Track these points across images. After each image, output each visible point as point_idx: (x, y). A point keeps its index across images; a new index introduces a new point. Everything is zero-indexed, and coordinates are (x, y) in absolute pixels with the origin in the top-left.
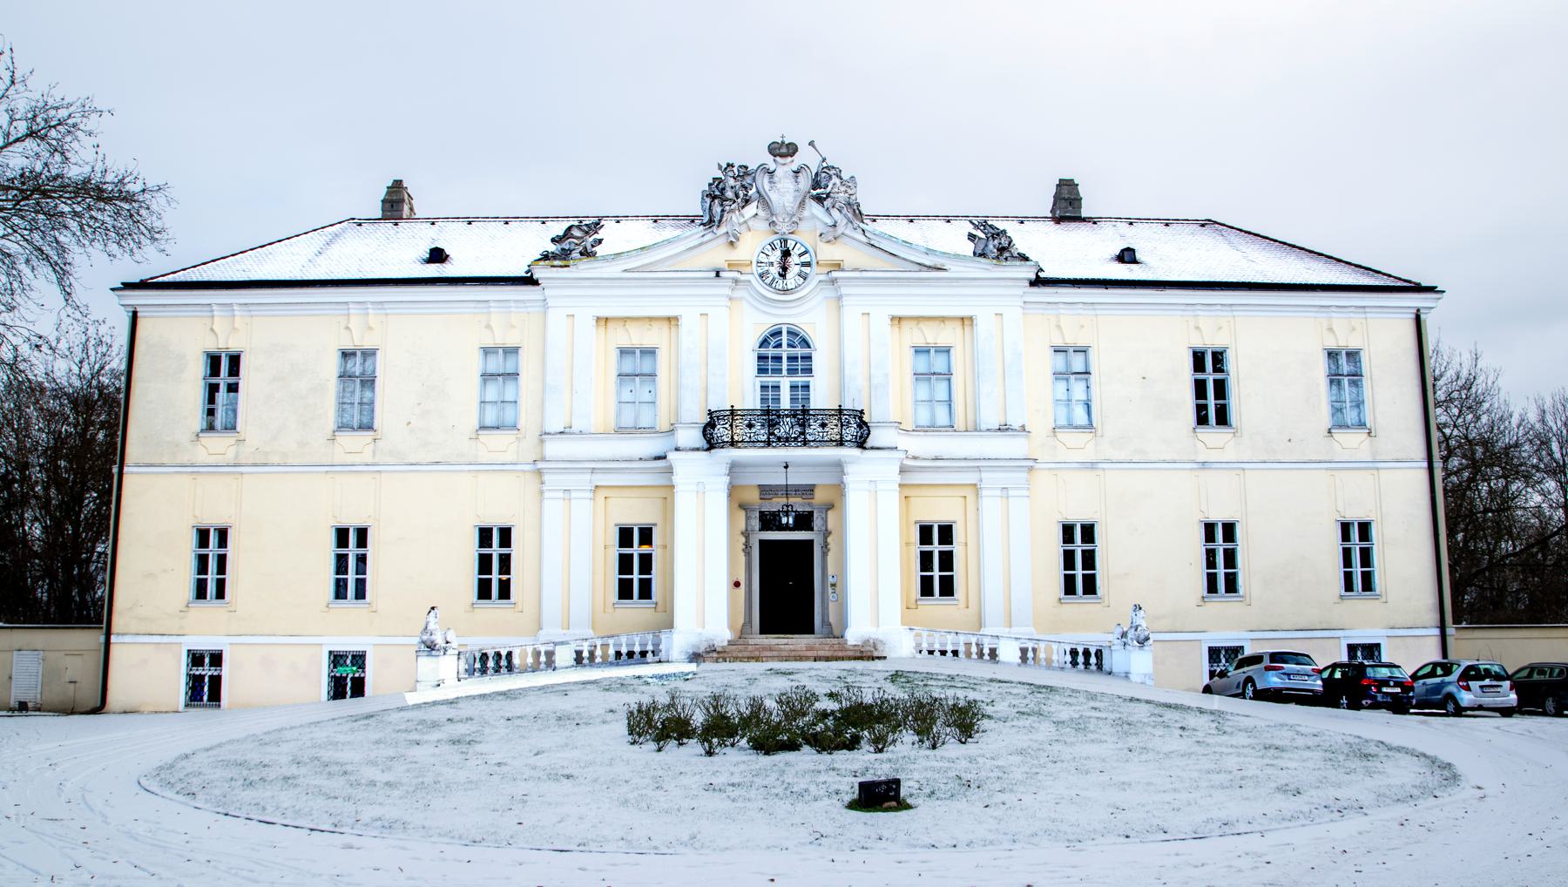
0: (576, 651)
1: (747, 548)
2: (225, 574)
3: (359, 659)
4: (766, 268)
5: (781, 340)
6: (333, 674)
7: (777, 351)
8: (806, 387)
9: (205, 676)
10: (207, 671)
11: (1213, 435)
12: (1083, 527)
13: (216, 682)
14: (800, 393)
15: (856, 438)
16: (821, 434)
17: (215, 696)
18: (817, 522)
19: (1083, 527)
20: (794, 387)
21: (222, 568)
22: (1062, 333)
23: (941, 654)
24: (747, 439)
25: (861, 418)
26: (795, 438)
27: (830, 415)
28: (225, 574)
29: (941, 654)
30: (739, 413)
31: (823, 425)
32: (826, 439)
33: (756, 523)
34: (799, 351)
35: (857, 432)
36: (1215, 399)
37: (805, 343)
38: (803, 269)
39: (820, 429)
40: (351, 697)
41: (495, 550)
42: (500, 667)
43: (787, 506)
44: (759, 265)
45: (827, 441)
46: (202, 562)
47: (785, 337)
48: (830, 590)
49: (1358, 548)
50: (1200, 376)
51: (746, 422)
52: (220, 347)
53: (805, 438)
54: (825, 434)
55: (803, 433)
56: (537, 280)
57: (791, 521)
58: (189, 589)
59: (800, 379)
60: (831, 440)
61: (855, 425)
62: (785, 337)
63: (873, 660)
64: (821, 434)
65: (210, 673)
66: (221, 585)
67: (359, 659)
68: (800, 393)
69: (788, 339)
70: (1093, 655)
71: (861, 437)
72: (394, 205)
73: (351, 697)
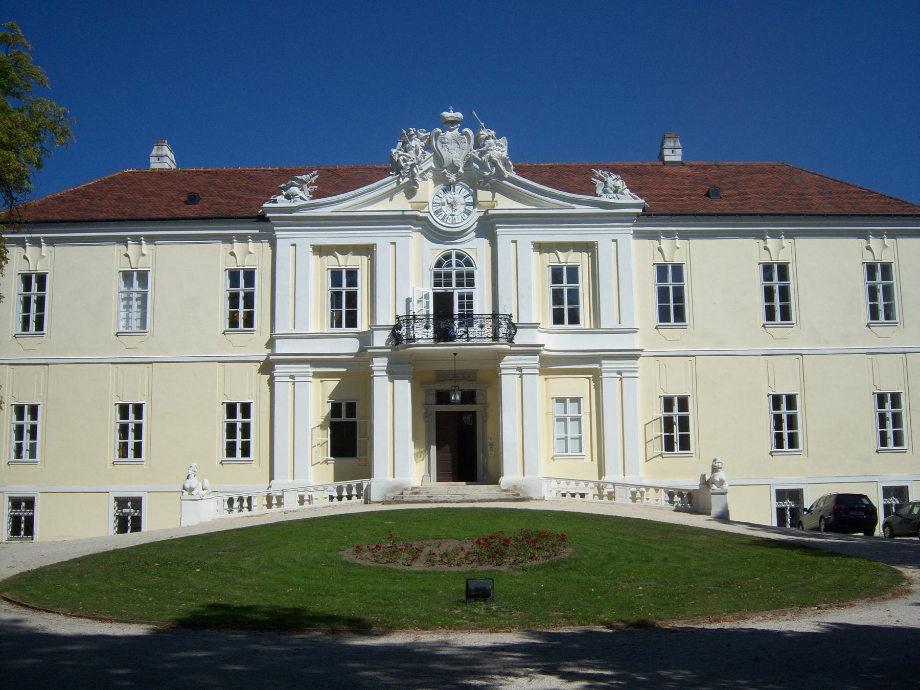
0: (9, 497)
1: (427, 415)
2: (141, 439)
3: (137, 503)
4: (439, 207)
5: (451, 261)
6: (117, 514)
7: (448, 269)
8: (470, 297)
9: (21, 516)
10: (23, 512)
11: (778, 330)
12: (348, 405)
13: (30, 521)
14: (465, 301)
15: (506, 335)
16: (480, 333)
17: (30, 531)
18: (479, 398)
19: (348, 405)
20: (461, 297)
21: (33, 435)
22: (873, 255)
23: (562, 496)
24: (425, 337)
25: (510, 320)
26: (461, 336)
27: (487, 318)
28: (141, 439)
29: (562, 496)
30: (419, 317)
31: (481, 326)
32: (483, 336)
33: (433, 399)
34: (465, 269)
35: (507, 331)
36: (780, 302)
37: (469, 263)
38: (467, 207)
39: (479, 329)
40: (131, 532)
41: (239, 419)
42: (243, 508)
43: (455, 387)
44: (434, 205)
45: (485, 338)
46: (124, 430)
47: (454, 259)
48: (489, 448)
49: (785, 415)
50: (557, 286)
51: (424, 324)
52: (31, 269)
53: (468, 336)
54: (483, 333)
55: (466, 332)
56: (269, 219)
57: (458, 398)
58: (113, 451)
59: (465, 290)
60: (488, 337)
61: (505, 326)
62: (454, 259)
63: (479, 500)
64: (480, 333)
65: (26, 514)
66: (33, 448)
67: (137, 503)
68: (465, 301)
69: (456, 261)
70: (245, 501)
71: (510, 335)
72: (160, 158)
73: (131, 532)
